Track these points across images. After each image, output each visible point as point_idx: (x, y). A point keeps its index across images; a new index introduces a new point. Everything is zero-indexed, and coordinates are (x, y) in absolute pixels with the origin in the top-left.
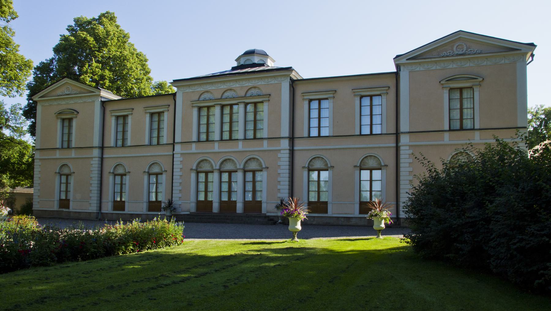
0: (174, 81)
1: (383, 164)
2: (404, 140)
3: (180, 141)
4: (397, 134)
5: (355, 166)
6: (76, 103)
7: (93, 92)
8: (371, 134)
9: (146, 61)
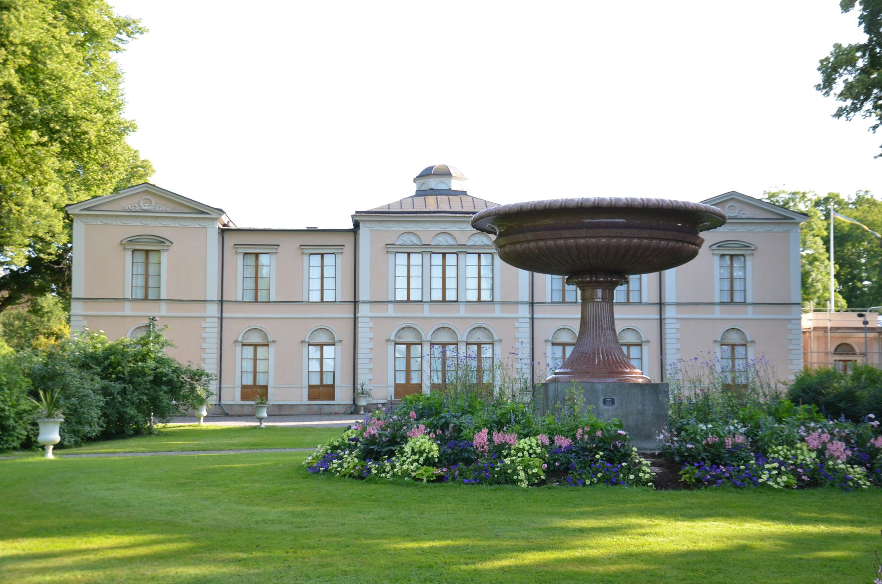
0: (357, 212)
1: (749, 340)
2: (670, 312)
3: (674, 301)
4: (355, 302)
5: (715, 341)
6: (165, 226)
7: (87, 209)
8: (409, 300)
9: (837, 196)
